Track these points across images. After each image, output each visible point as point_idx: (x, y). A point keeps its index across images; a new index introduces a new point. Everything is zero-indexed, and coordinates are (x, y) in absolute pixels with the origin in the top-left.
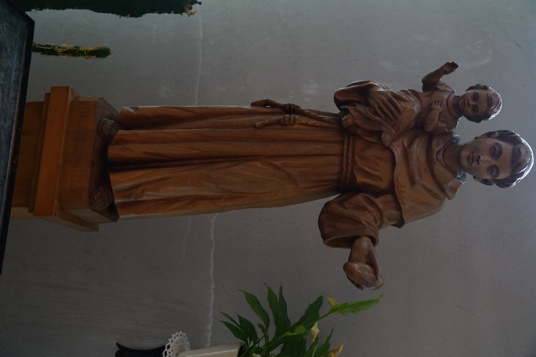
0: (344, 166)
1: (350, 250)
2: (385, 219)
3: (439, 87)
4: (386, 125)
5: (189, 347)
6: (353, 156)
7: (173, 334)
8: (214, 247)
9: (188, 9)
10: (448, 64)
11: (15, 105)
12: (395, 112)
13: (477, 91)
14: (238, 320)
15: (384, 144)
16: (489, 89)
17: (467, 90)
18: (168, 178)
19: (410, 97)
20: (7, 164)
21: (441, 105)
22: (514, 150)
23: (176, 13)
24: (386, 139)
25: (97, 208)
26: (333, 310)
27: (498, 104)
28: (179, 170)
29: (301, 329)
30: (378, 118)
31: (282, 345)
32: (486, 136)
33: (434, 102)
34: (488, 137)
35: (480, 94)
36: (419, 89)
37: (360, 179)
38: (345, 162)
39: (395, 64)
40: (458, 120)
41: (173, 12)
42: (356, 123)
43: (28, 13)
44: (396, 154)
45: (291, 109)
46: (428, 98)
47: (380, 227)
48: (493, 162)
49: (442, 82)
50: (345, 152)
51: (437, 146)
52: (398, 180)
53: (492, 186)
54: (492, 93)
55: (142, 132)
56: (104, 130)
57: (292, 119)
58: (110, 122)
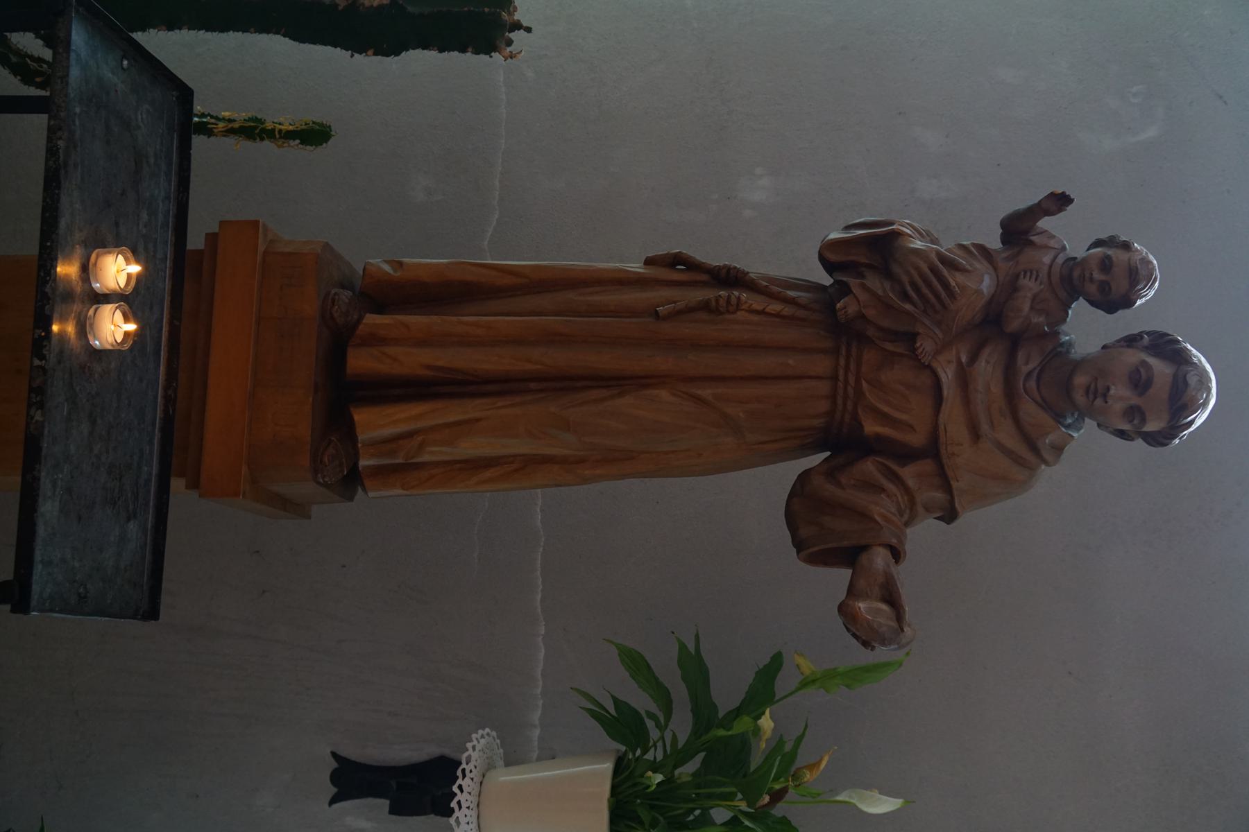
0: (840, 401)
1: (850, 571)
2: (920, 509)
3: (1033, 238)
4: (927, 322)
5: (501, 759)
6: (858, 381)
7: (475, 733)
8: (542, 544)
9: (503, 46)
10: (1052, 195)
11: (165, 273)
12: (943, 294)
13: (1110, 252)
14: (613, 706)
15: (920, 359)
16: (1133, 250)
17: (1088, 250)
18: (477, 420)
19: (975, 263)
20: (156, 397)
21: (1036, 279)
22: (1175, 376)
23: (477, 52)
24: (924, 349)
25: (326, 480)
26: (805, 684)
27: (1150, 279)
28: (499, 404)
29: (742, 725)
30: (908, 307)
31: (702, 755)
32: (1125, 344)
33: (1023, 273)
34: (1128, 346)
35: (1114, 259)
36: (994, 241)
37: (871, 427)
38: (841, 392)
39: (947, 137)
40: (1070, 307)
41: (470, 49)
42: (863, 314)
43: (138, 36)
44: (943, 380)
45: (729, 278)
46: (1011, 263)
47: (907, 524)
48: (1135, 401)
49: (1042, 228)
50: (841, 373)
51: (1027, 363)
52: (946, 432)
53: (1133, 442)
54: (1140, 257)
55: (417, 321)
56: (336, 315)
57: (734, 301)
58: (345, 295)
